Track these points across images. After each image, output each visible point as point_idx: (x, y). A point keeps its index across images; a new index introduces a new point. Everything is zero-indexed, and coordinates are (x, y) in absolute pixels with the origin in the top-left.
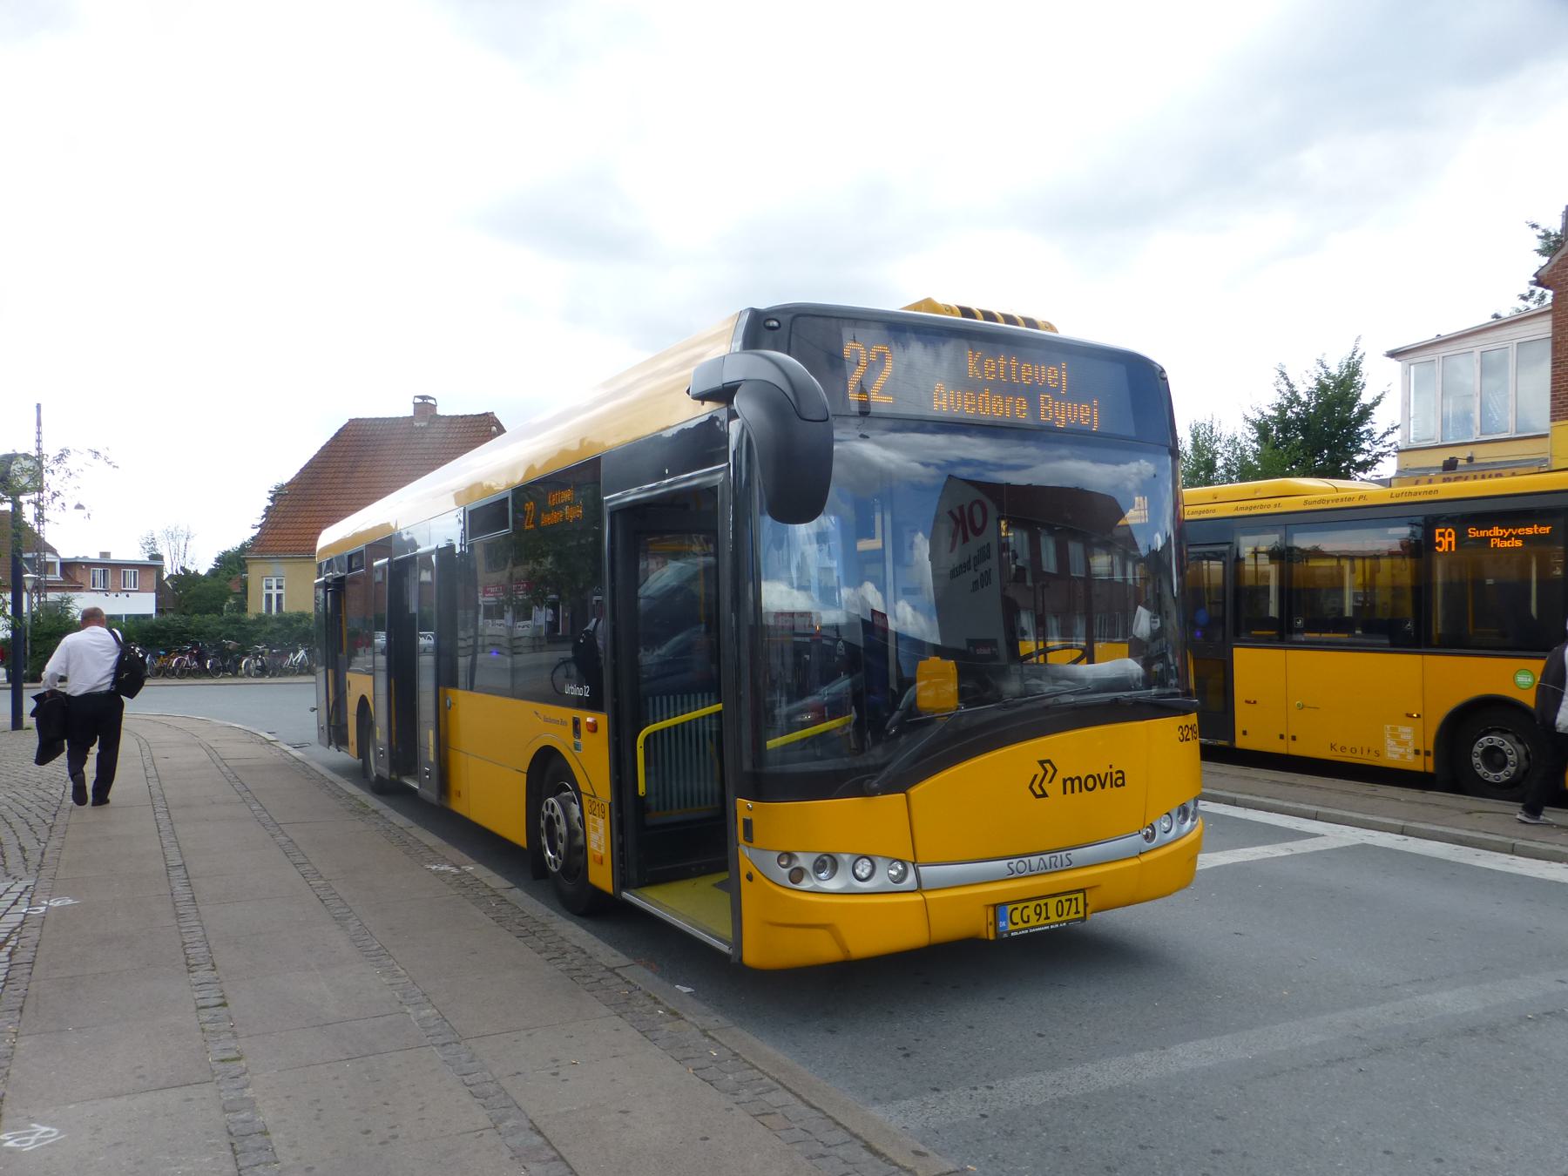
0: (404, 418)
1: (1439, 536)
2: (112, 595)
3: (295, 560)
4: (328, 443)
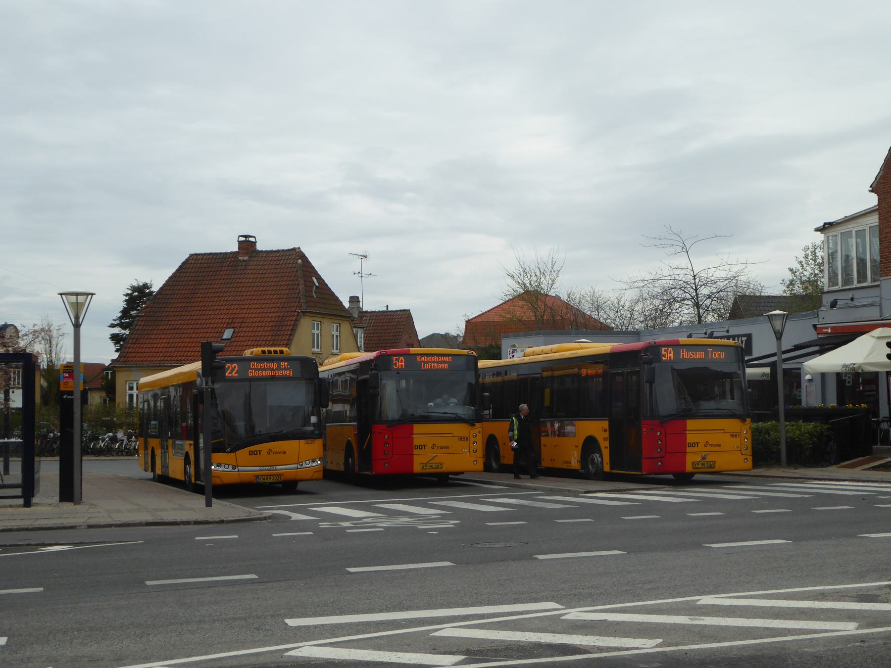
1: (396, 361)
3: (149, 368)
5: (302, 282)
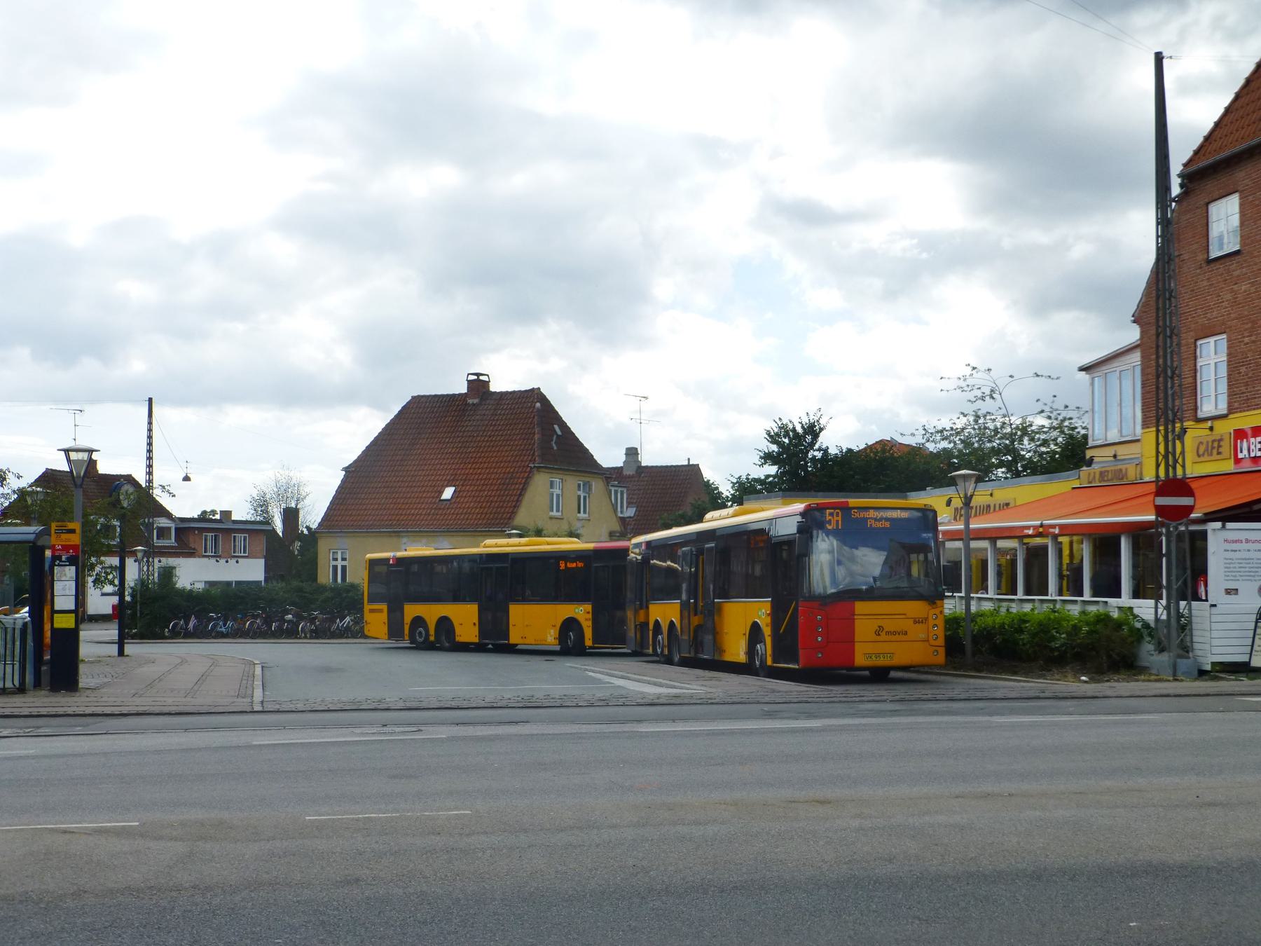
2: (223, 561)
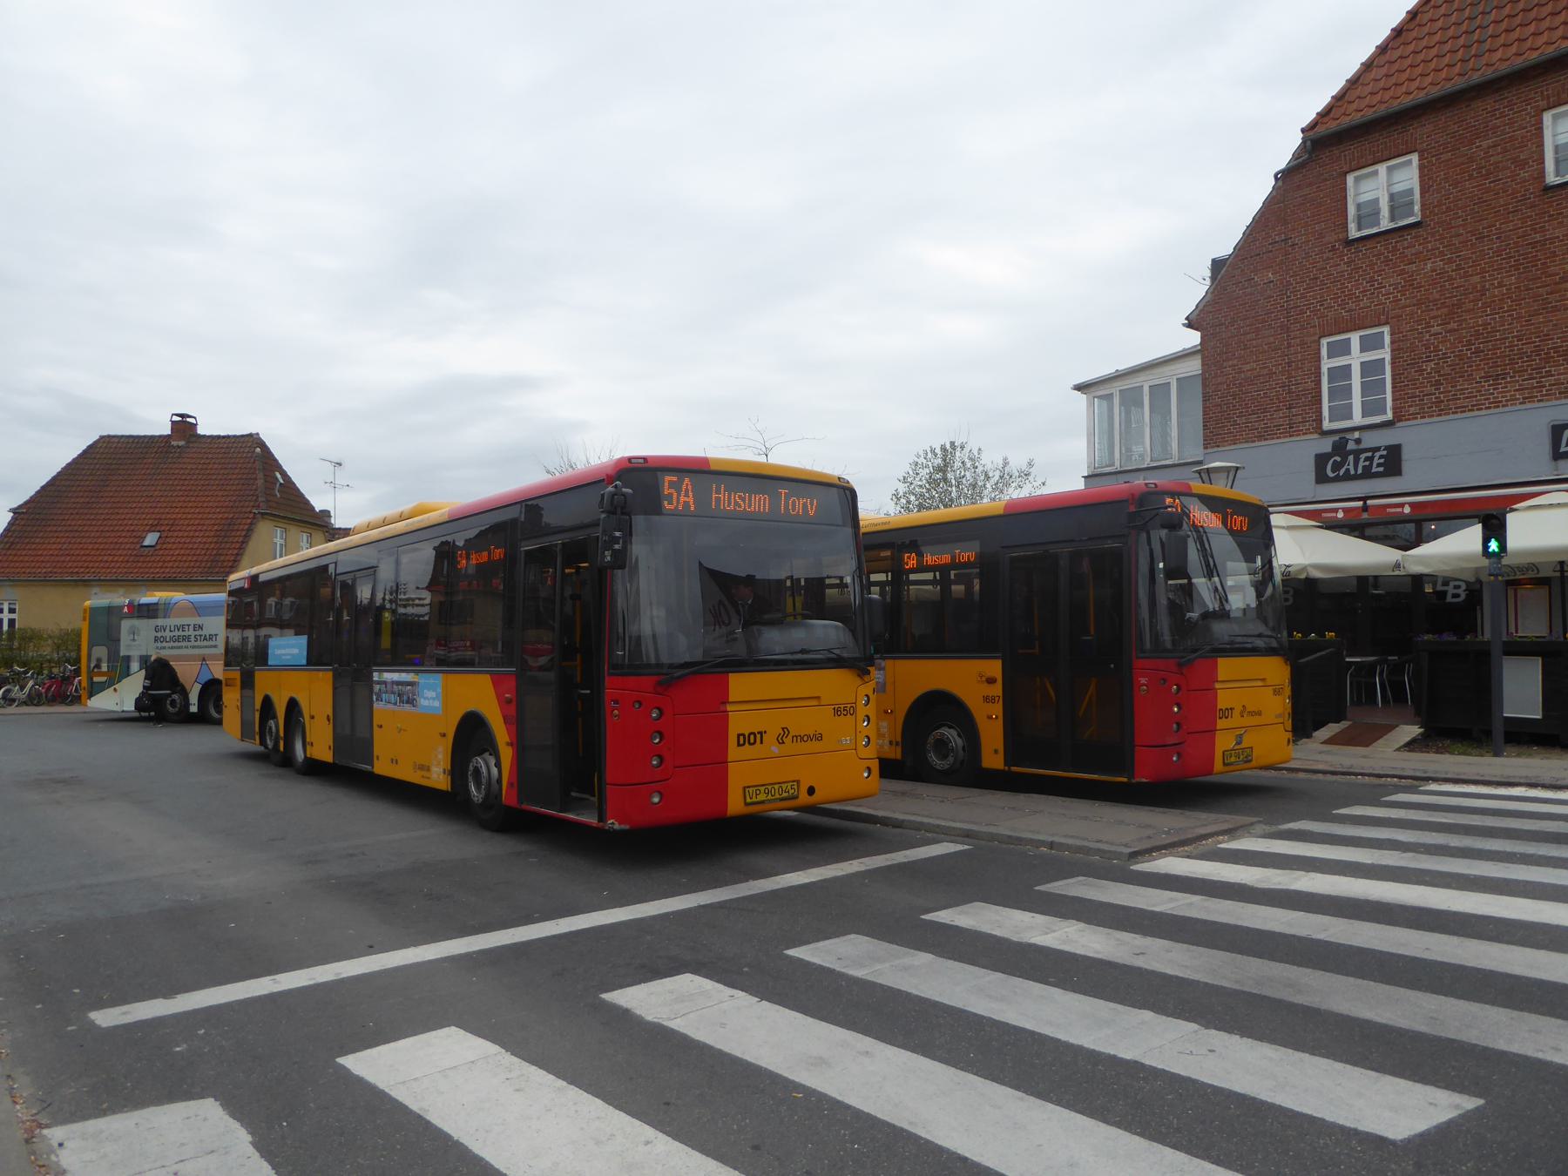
0: (160, 436)
4: (74, 460)
5: (261, 475)
